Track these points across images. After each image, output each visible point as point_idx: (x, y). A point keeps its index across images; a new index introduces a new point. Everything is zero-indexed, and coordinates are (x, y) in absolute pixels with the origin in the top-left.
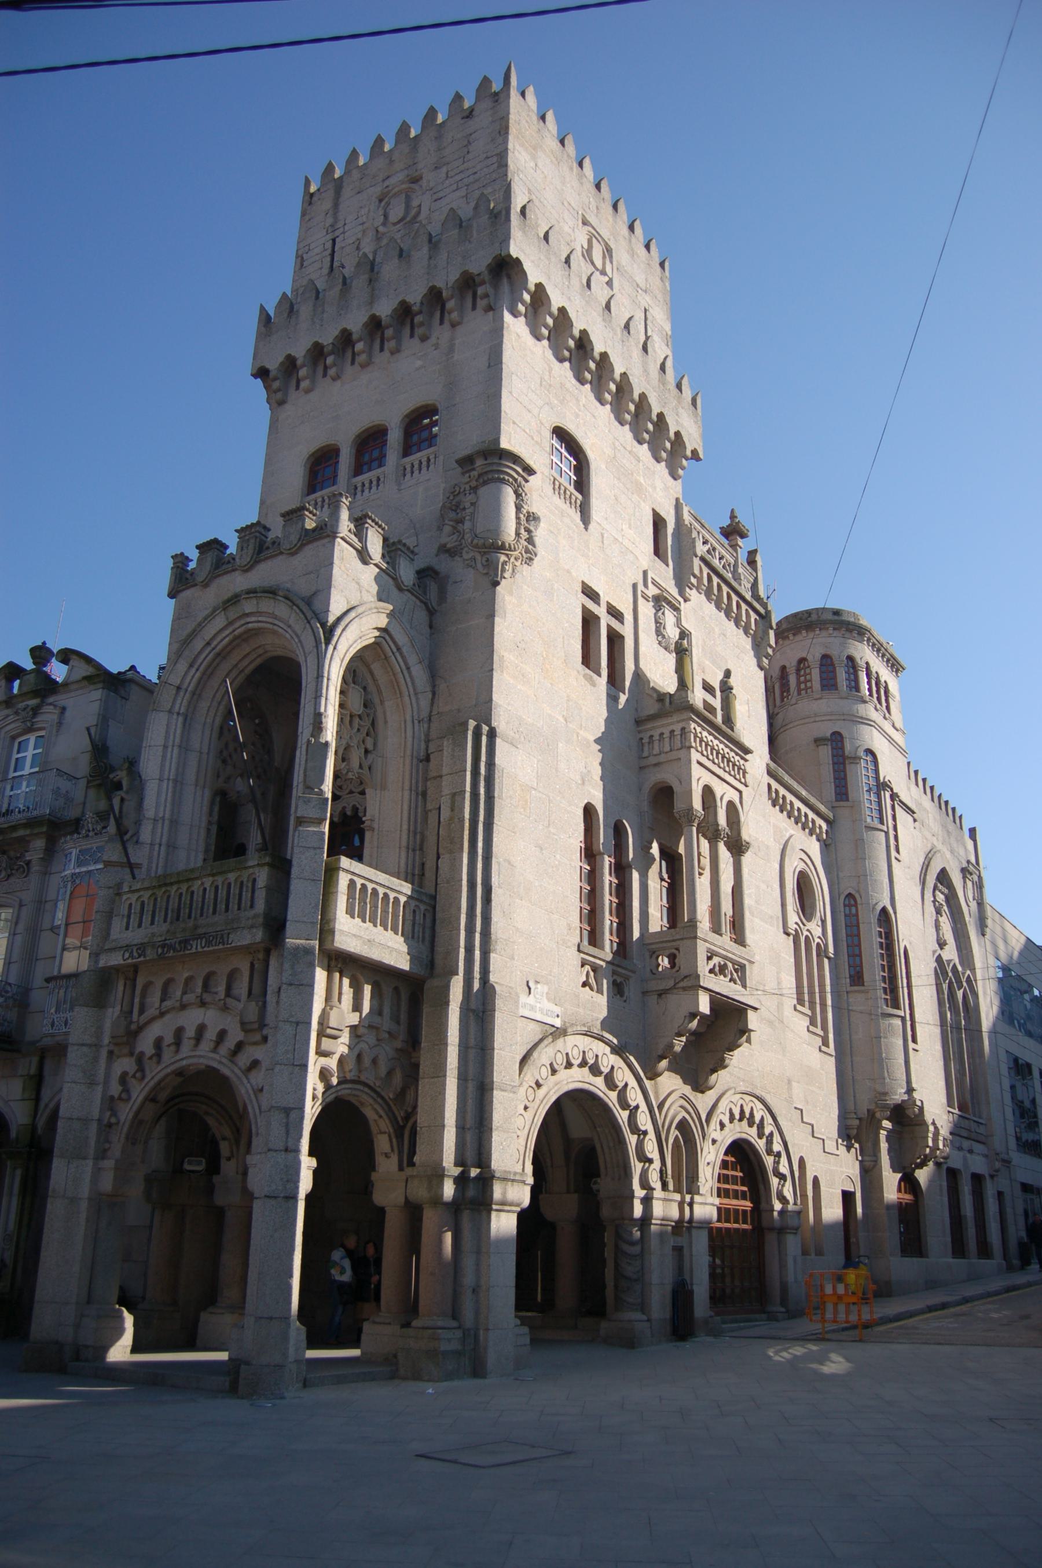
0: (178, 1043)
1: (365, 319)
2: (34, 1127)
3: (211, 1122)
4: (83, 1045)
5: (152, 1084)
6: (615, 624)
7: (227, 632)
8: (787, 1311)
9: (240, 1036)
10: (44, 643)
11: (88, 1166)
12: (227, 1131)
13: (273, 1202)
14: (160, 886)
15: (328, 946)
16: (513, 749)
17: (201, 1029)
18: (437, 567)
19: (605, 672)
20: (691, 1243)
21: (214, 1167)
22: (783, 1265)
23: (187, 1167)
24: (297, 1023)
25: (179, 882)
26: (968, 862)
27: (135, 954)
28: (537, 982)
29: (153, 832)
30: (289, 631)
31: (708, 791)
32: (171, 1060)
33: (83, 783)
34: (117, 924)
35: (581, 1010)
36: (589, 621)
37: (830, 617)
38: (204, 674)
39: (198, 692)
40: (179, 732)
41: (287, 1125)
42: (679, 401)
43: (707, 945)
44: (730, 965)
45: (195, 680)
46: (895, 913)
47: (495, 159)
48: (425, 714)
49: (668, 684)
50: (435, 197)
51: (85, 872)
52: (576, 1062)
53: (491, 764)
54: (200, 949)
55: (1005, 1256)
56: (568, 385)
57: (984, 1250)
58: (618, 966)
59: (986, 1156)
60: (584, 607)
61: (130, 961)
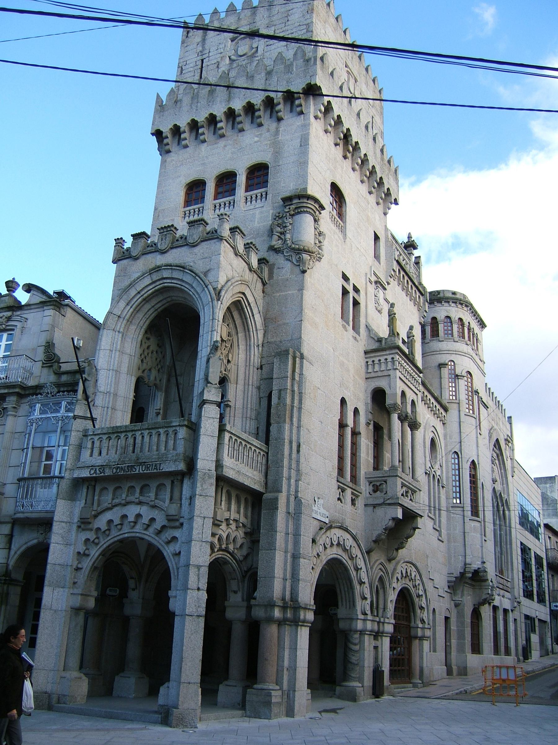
1: (225, 110)
2: (7, 565)
4: (63, 522)
7: (151, 287)
8: (422, 683)
9: (165, 523)
10: (14, 279)
14: (113, 433)
16: (311, 366)
17: (139, 516)
18: (267, 258)
19: (351, 323)
20: (382, 644)
21: (124, 594)
22: (421, 658)
24: (204, 518)
25: (126, 431)
26: (508, 436)
27: (98, 471)
28: (319, 498)
30: (192, 290)
31: (403, 394)
34: (86, 454)
37: (450, 295)
38: (134, 310)
39: (130, 320)
41: (198, 575)
42: (390, 170)
44: (410, 491)
46: (479, 464)
49: (383, 332)
51: (45, 418)
52: (335, 543)
53: (301, 374)
54: (141, 472)
55: (517, 655)
56: (338, 159)
57: (507, 652)
58: (354, 490)
59: (510, 599)
61: (94, 475)
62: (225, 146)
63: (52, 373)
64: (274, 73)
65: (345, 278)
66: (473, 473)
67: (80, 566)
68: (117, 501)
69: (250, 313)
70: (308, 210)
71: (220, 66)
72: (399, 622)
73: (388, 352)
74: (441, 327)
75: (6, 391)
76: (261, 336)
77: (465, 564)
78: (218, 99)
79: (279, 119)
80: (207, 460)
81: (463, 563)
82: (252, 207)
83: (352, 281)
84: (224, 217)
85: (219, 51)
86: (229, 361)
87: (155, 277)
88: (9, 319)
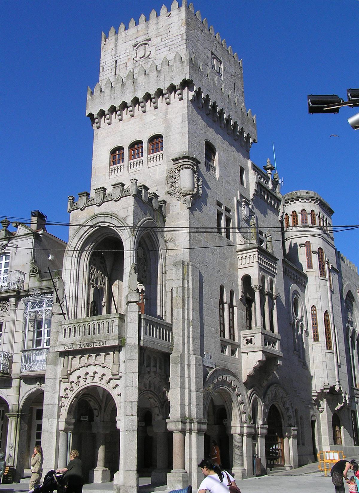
3: (91, 403)
5: (77, 392)
6: (227, 214)
12: (97, 407)
13: (129, 432)
21: (91, 419)
23: (82, 419)
33: (27, 276)
47: (180, 36)
50: (157, 49)
62: (135, 123)
63: (37, 281)
64: (162, 72)
65: (219, 204)
68: (81, 365)
70: (185, 166)
71: (128, 65)
73: (251, 251)
74: (299, 218)
75: (8, 294)
78: (128, 91)
82: (154, 165)
85: (127, 54)
86: (144, 271)
88: (6, 245)
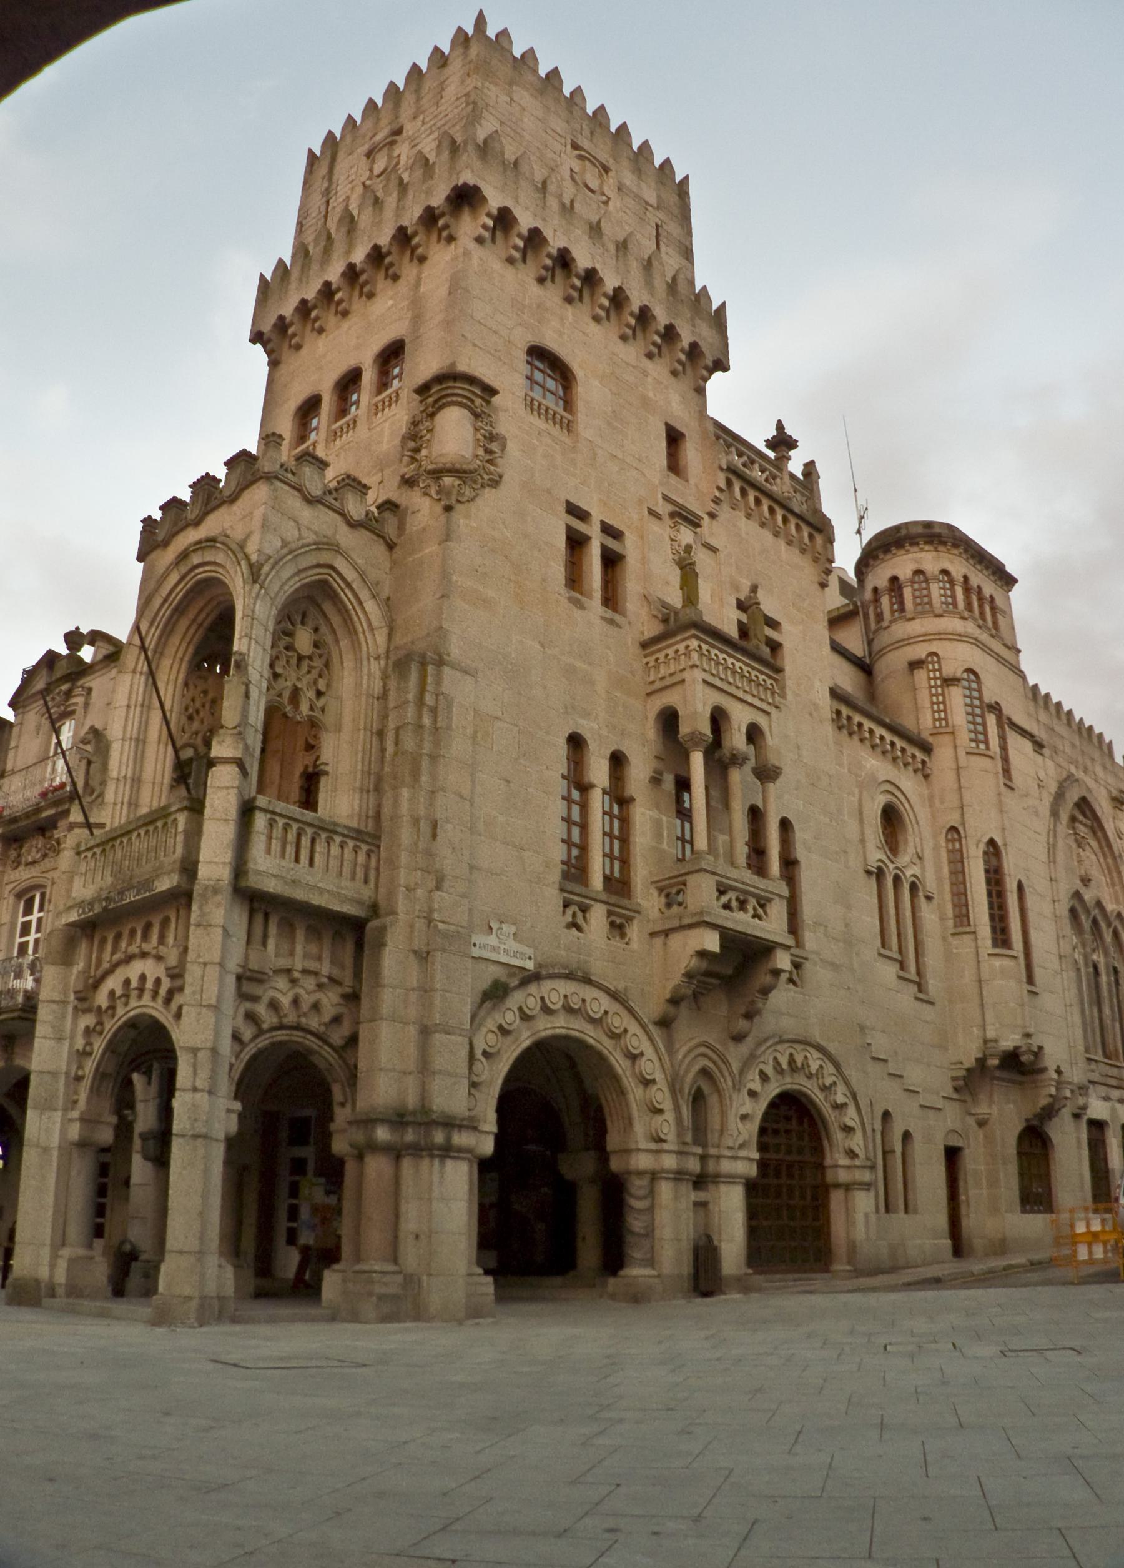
0: (126, 996)
10: (77, 628)
11: (58, 1116)
15: (243, 884)
17: (143, 978)
24: (205, 964)
29: (116, 793)
32: (124, 1014)
35: (563, 953)
36: (576, 542)
37: (920, 530)
39: (159, 650)
40: (141, 690)
43: (717, 878)
45: (155, 638)
48: (382, 650)
58: (614, 905)
60: (569, 528)
66: (994, 862)
67: (80, 1073)
69: (353, 599)
72: (767, 1156)
76: (381, 638)
77: (986, 1041)
79: (422, 259)
80: (216, 863)
81: (981, 1041)
83: (597, 516)
84: (271, 439)
87: (183, 569)
